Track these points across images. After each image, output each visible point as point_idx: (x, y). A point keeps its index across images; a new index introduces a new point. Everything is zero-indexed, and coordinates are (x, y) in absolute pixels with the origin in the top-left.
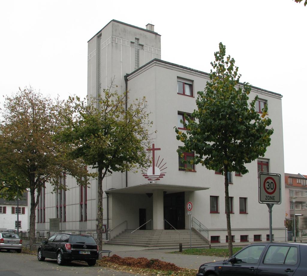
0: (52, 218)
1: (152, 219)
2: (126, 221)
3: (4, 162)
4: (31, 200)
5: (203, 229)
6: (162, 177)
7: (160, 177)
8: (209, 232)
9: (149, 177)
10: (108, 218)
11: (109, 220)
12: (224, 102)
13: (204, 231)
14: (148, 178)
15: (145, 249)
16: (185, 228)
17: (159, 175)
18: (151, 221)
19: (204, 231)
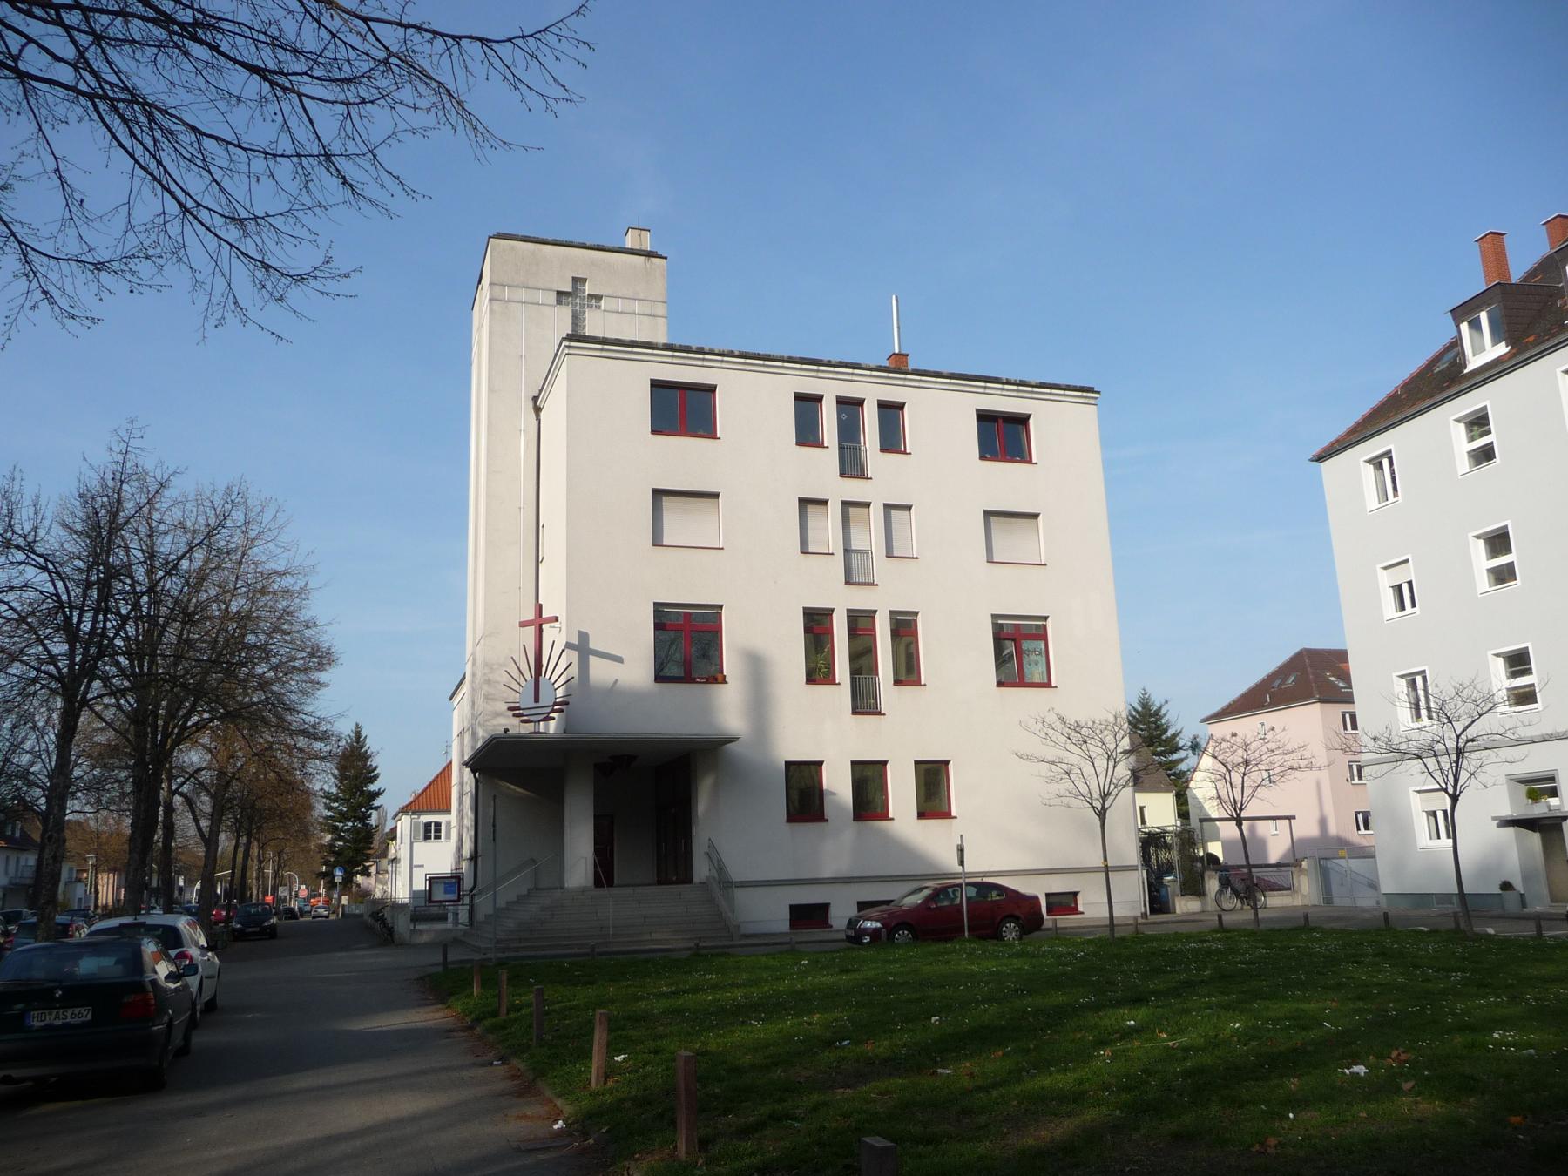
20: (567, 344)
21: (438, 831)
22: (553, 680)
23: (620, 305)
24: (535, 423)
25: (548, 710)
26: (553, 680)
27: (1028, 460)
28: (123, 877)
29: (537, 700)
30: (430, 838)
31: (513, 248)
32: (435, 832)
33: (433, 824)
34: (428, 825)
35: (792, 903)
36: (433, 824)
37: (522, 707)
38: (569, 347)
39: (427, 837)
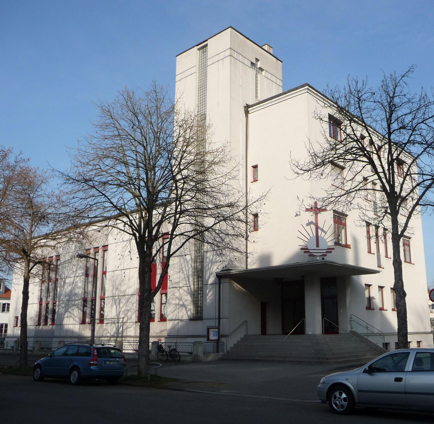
0: (164, 322)
1: (305, 318)
2: (246, 321)
3: (150, 188)
4: (426, 261)
5: (383, 333)
6: (331, 252)
7: (327, 252)
8: (385, 336)
9: (311, 251)
10: (219, 316)
11: (221, 320)
12: (217, 227)
13: (376, 335)
14: (309, 252)
15: (42, 315)
16: (204, 318)
17: (327, 249)
18: (304, 320)
19: (376, 335)
20: (308, 87)
21: (8, 308)
22: (309, 238)
23: (269, 76)
24: (245, 119)
25: (325, 251)
26: (309, 238)
27: (257, 165)
28: (132, 357)
29: (318, 245)
30: (5, 311)
31: (237, 36)
32: (5, 307)
33: (7, 304)
34: (4, 305)
35: (154, 322)
36: (7, 304)
37: (309, 248)
38: (308, 89)
39: (3, 310)
